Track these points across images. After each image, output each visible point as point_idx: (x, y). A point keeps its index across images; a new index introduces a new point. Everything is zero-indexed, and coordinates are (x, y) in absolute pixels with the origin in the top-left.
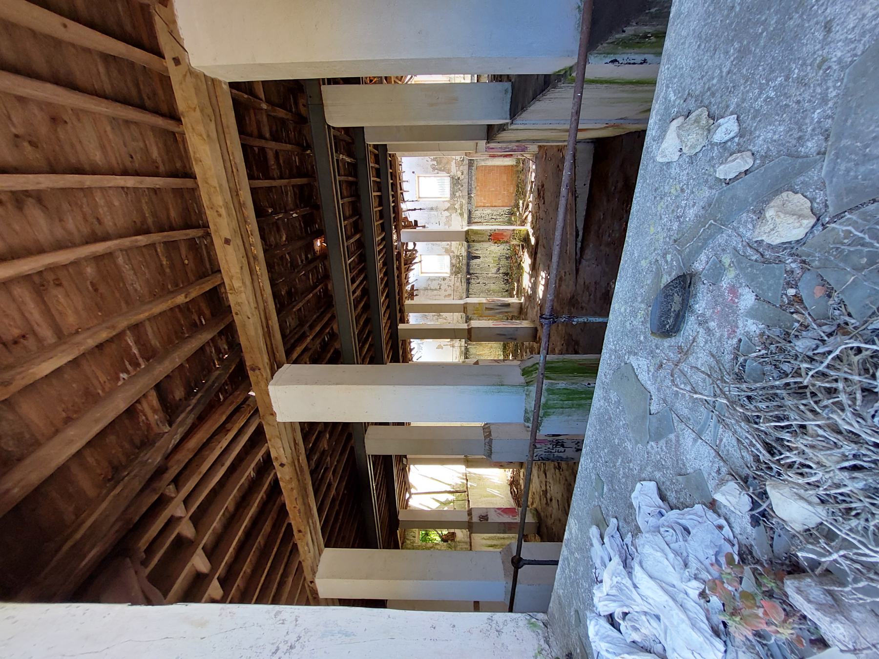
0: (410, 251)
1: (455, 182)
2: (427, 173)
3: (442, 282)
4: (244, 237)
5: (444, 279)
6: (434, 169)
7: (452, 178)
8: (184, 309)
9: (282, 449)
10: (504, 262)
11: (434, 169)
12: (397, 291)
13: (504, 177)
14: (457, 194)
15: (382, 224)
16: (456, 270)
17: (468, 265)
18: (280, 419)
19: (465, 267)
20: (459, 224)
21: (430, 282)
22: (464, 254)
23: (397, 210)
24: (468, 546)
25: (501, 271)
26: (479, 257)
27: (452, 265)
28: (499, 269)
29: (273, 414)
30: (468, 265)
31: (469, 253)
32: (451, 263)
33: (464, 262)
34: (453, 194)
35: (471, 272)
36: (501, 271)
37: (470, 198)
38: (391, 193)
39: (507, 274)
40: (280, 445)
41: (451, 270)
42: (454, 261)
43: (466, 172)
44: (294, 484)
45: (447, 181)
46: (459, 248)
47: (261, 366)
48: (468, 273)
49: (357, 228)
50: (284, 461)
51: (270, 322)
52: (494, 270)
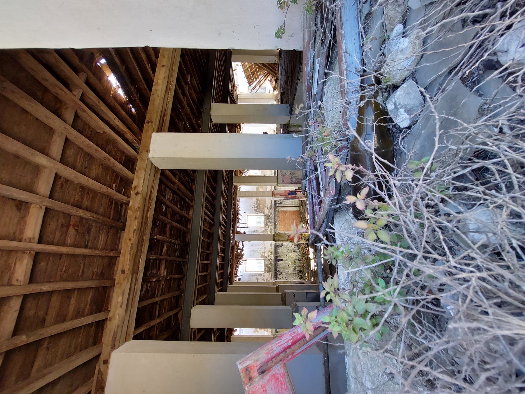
0: (240, 249)
1: (267, 218)
2: (252, 213)
3: (259, 277)
4: (171, 70)
5: (260, 275)
6: (256, 211)
7: (266, 216)
8: (94, 194)
9: (142, 179)
10: (297, 263)
11: (256, 211)
12: (226, 335)
13: (293, 216)
14: (269, 224)
15: (223, 265)
16: (268, 269)
17: (276, 265)
18: (151, 155)
19: (273, 267)
20: (271, 231)
21: (251, 277)
22: (273, 258)
23: (234, 226)
24: (276, 180)
25: (297, 270)
26: (282, 260)
27: (266, 266)
28: (295, 268)
29: (148, 151)
30: (276, 265)
31: (276, 257)
32: (265, 264)
33: (273, 263)
34: (266, 224)
35: (278, 270)
36: (297, 270)
37: (275, 225)
38: (231, 228)
39: (300, 272)
40: (143, 176)
41: (265, 269)
42: (267, 263)
43: (273, 213)
44: (139, 214)
45: (263, 219)
46: (270, 244)
47: (154, 121)
48: (276, 270)
49: (205, 268)
50: (140, 189)
51: (165, 117)
52: (292, 269)
